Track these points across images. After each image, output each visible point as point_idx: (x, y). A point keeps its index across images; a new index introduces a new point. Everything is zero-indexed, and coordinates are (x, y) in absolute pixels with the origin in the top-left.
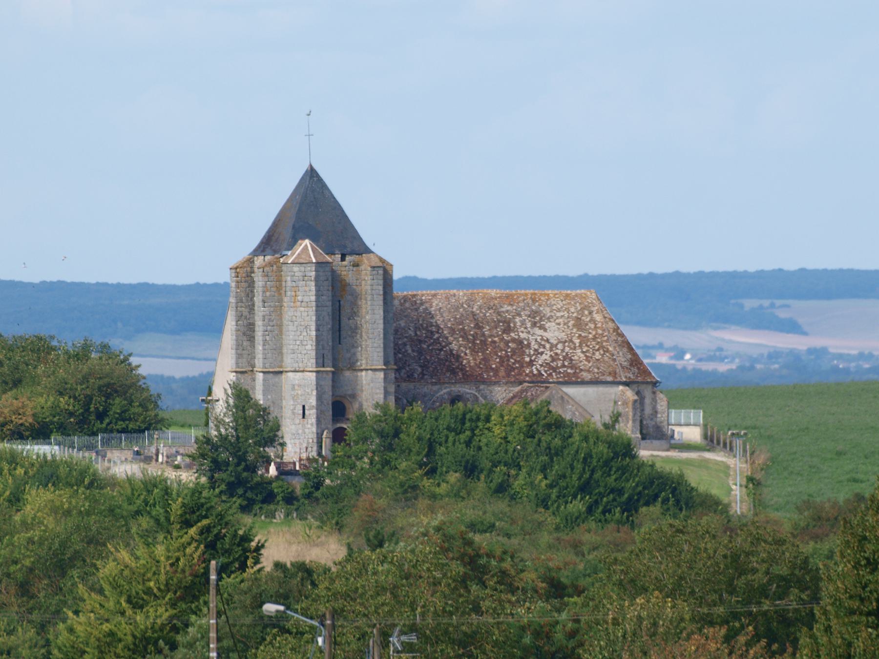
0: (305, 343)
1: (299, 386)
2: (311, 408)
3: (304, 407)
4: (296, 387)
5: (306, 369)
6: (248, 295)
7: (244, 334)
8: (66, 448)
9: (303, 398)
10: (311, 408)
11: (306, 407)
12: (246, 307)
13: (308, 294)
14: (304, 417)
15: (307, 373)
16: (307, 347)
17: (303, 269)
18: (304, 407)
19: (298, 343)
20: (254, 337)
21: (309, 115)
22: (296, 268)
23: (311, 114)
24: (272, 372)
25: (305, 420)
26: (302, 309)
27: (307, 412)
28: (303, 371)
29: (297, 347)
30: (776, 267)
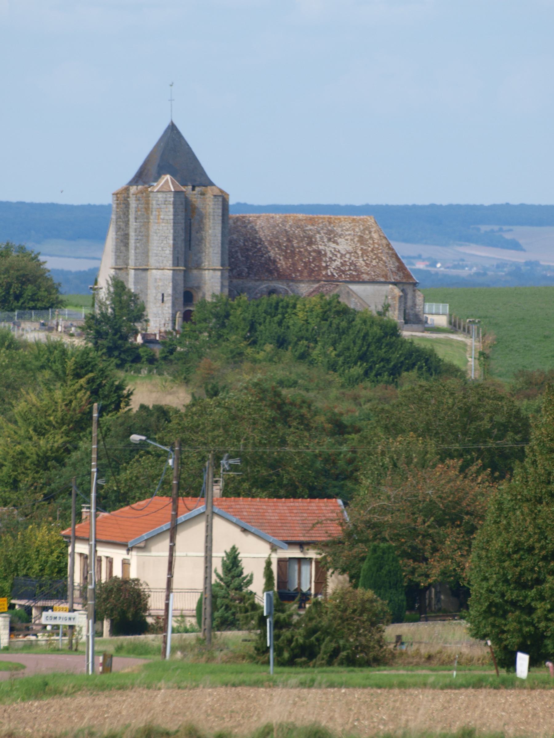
3: (163, 295)
6: (124, 214)
7: (122, 241)
11: (165, 295)
17: (164, 196)
18: (163, 295)
22: (160, 195)
26: (163, 224)
27: (165, 299)
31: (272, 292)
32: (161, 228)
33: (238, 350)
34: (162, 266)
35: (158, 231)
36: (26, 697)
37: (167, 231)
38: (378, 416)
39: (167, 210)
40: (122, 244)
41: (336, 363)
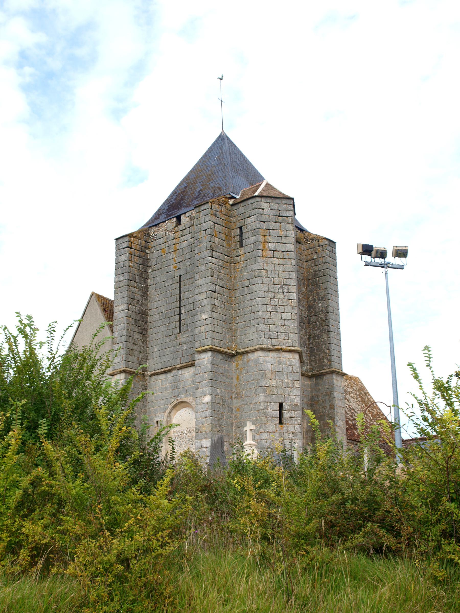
0: (281, 309)
1: (272, 372)
2: (294, 407)
3: (281, 405)
4: (269, 374)
5: (284, 348)
6: (141, 275)
7: (136, 324)
8: (46, 431)
9: (280, 391)
10: (294, 407)
11: (285, 406)
12: (139, 289)
13: (284, 240)
14: (281, 423)
15: (286, 355)
16: (284, 316)
17: (275, 206)
18: (281, 405)
19: (270, 308)
20: (146, 330)
21: (221, 79)
22: (265, 204)
23: (223, 78)
24: (225, 353)
25: (285, 427)
26: (276, 261)
27: (286, 414)
28: (279, 350)
29: (269, 314)
30: (356, 376)
31: (385, 599)
32: (270, 267)
33: (128, 510)
34: (276, 343)
35: (264, 273)
36: (450, 500)
37: (285, 274)
38: (78, 498)
39: (282, 233)
40: (136, 329)
41: (106, 572)
